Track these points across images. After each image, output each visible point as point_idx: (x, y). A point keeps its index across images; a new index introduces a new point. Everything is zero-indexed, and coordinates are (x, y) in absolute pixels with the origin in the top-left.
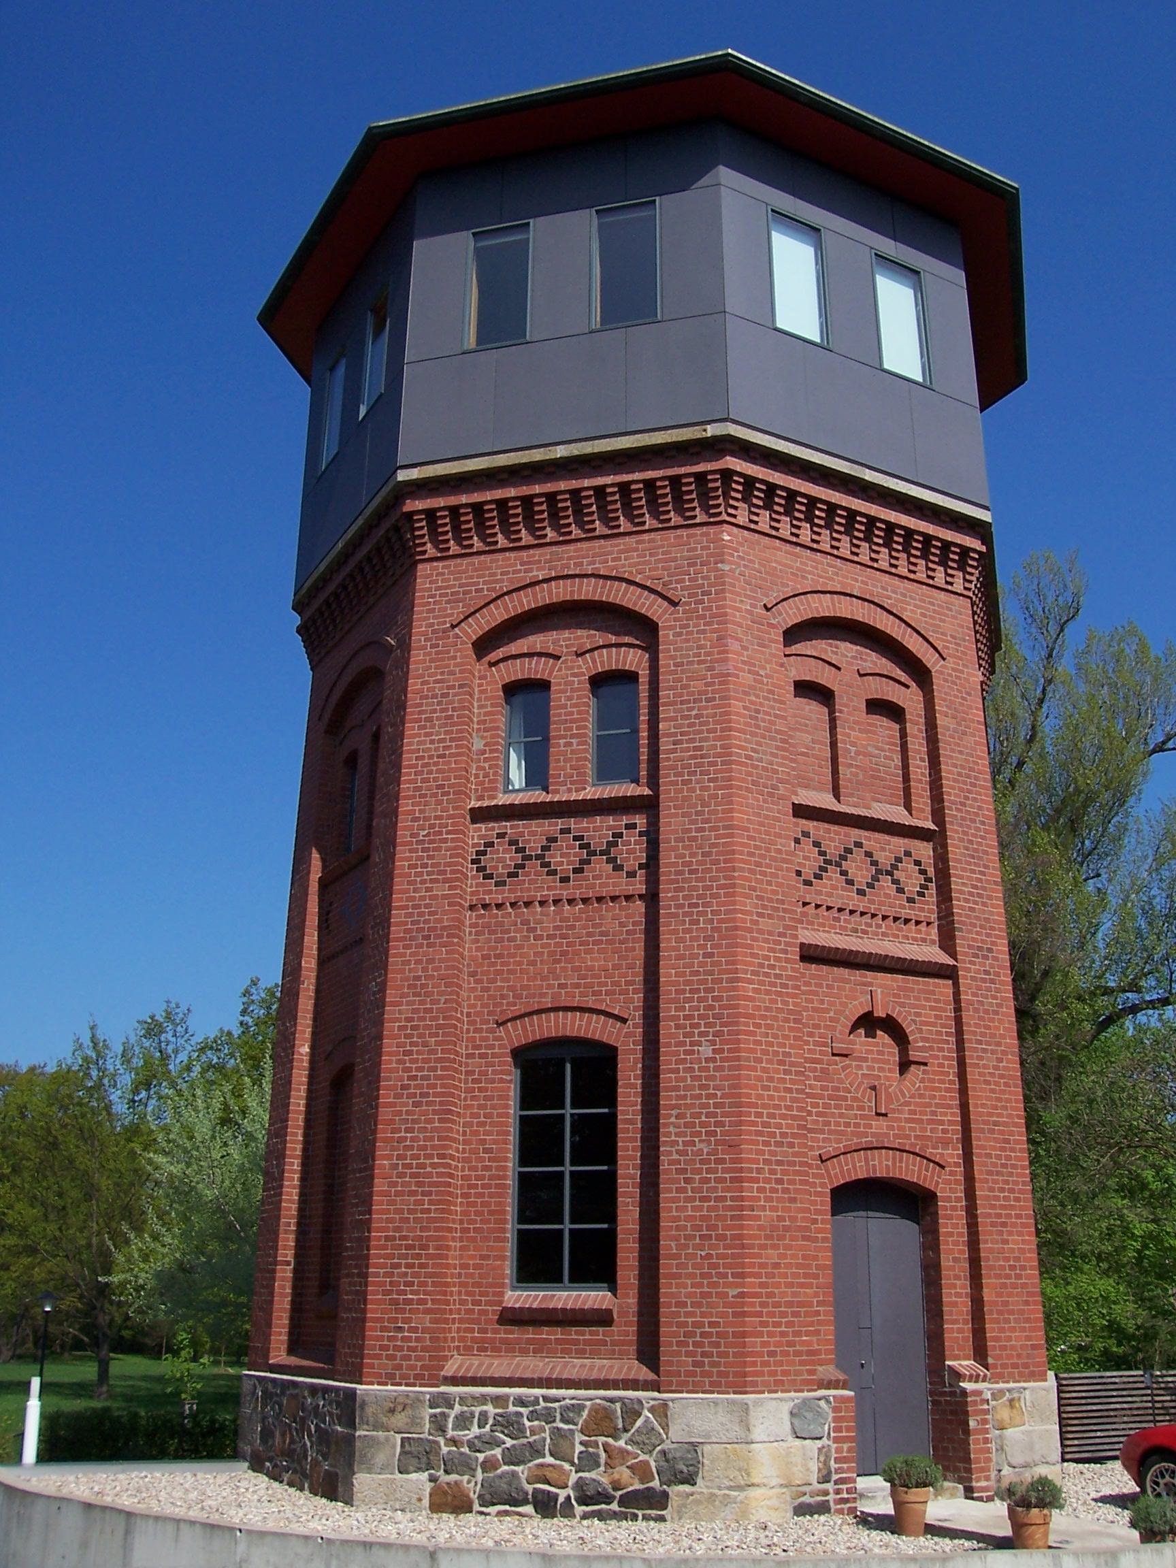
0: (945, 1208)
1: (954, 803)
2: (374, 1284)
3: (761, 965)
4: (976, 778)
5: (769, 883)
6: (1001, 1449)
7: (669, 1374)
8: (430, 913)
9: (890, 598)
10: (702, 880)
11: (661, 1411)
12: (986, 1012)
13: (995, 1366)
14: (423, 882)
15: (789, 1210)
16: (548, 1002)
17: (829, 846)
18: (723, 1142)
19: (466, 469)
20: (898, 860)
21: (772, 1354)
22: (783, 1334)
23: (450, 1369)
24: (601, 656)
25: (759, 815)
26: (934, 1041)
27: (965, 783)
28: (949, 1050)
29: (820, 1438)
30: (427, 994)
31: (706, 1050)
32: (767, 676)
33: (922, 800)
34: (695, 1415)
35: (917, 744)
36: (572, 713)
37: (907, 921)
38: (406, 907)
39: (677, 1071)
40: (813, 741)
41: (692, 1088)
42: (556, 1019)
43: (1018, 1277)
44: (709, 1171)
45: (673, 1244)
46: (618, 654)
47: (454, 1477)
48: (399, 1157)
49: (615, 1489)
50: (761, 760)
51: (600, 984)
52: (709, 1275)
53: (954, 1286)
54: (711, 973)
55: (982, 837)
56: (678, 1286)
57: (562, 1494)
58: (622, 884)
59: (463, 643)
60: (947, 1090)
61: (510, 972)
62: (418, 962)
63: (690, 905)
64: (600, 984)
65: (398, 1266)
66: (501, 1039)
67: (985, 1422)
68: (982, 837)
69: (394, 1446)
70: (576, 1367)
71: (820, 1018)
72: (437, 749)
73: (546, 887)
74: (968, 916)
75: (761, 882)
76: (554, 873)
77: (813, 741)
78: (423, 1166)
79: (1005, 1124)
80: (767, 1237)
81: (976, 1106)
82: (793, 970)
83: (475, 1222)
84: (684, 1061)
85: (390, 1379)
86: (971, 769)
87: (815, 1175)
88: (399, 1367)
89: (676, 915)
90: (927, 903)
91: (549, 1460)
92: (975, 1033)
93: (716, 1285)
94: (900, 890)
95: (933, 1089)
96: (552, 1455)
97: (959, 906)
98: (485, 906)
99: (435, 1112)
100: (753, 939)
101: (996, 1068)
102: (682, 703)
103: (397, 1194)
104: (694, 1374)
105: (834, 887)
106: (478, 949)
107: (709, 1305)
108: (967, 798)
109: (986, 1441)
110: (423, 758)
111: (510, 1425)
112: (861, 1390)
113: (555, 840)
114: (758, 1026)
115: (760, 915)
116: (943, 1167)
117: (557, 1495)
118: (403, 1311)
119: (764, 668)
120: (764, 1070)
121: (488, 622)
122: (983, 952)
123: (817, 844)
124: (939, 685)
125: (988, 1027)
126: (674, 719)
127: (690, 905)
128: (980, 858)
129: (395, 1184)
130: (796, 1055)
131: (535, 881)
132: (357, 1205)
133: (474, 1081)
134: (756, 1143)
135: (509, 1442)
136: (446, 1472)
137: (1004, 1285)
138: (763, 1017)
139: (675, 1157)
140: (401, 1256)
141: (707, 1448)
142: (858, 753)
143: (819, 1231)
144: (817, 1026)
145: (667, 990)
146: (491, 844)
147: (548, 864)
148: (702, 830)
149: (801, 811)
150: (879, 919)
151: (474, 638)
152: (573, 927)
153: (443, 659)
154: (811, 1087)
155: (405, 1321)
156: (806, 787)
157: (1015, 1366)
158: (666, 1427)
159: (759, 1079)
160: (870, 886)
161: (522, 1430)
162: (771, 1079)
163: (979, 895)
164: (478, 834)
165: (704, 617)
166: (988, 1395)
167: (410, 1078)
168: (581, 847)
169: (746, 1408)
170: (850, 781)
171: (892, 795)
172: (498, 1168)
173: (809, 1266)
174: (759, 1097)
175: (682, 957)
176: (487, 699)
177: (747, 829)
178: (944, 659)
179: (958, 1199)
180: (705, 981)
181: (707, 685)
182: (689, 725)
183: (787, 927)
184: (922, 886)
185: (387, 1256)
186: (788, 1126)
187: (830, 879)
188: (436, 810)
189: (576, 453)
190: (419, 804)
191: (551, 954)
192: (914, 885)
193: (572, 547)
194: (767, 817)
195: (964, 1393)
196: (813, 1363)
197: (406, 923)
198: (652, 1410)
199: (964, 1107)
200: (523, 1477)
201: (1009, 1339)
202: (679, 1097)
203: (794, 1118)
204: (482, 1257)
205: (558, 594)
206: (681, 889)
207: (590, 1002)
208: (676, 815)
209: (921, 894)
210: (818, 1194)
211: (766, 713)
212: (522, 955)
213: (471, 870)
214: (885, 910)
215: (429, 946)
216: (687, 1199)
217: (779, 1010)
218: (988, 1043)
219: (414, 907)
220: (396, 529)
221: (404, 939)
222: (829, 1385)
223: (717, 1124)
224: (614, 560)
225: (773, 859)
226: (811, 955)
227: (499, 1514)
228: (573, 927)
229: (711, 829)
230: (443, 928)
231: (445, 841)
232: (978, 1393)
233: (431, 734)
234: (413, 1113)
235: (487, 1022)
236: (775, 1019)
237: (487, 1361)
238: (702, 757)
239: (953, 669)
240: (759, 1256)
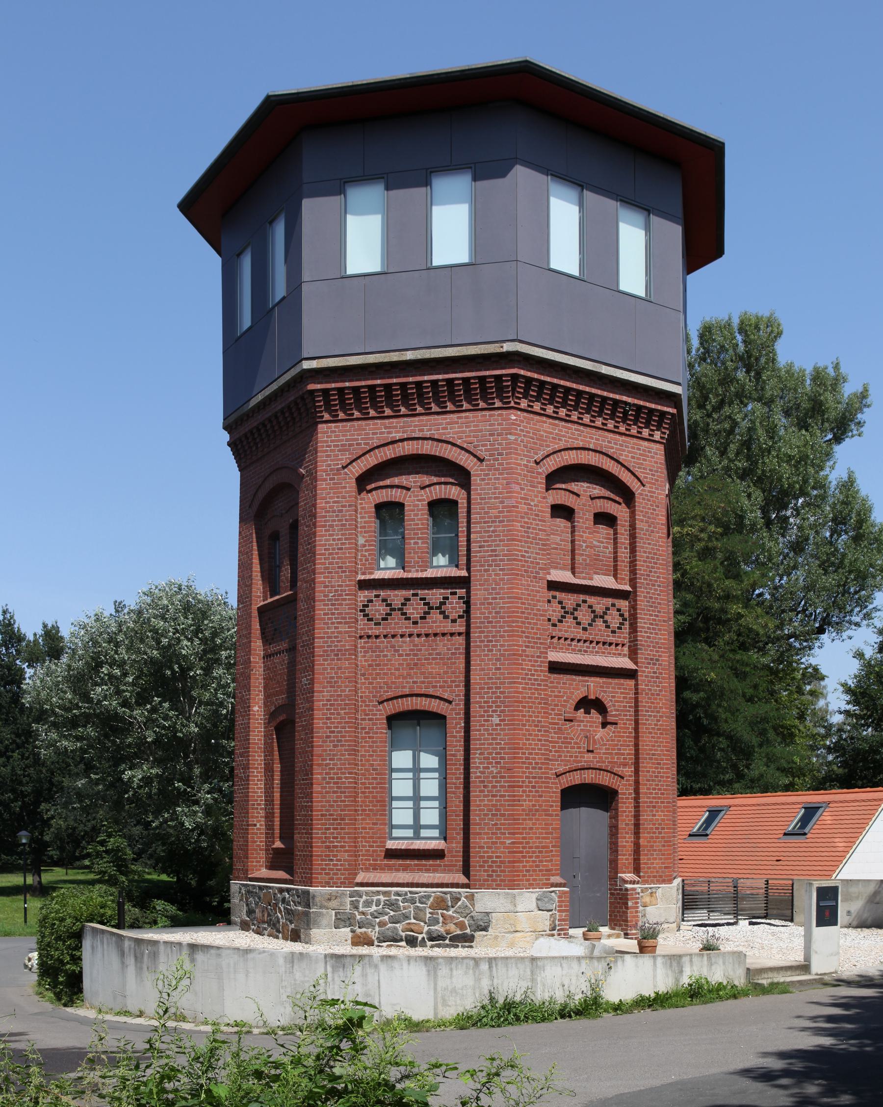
0: (622, 798)
1: (643, 575)
2: (316, 838)
3: (527, 674)
4: (658, 559)
5: (533, 628)
6: (644, 916)
7: (475, 880)
8: (338, 641)
9: (612, 448)
10: (495, 627)
11: (471, 898)
12: (653, 694)
13: (644, 877)
14: (333, 623)
15: (537, 801)
16: (407, 691)
17: (567, 604)
18: (504, 768)
19: (348, 364)
20: (608, 609)
21: (528, 871)
22: (533, 862)
23: (359, 878)
24: (435, 489)
25: (527, 590)
26: (622, 711)
27: (650, 562)
28: (630, 716)
29: (551, 910)
30: (339, 687)
31: (496, 720)
32: (535, 505)
33: (625, 573)
34: (488, 900)
35: (624, 539)
36: (418, 524)
37: (610, 644)
38: (323, 638)
39: (480, 730)
40: (561, 540)
41: (487, 739)
42: (412, 701)
43: (660, 833)
44: (496, 782)
45: (477, 818)
46: (446, 489)
47: (364, 930)
48: (327, 774)
49: (447, 934)
50: (530, 557)
51: (436, 682)
52: (496, 834)
53: (625, 838)
54: (499, 678)
55: (658, 595)
56: (480, 838)
57: (420, 937)
58: (449, 627)
59: (350, 478)
60: (627, 737)
61: (385, 674)
62: (332, 669)
63: (488, 641)
64: (436, 682)
65: (329, 829)
66: (380, 710)
67: (637, 903)
68: (658, 595)
69: (331, 916)
70: (425, 877)
71: (559, 701)
72: (337, 544)
73: (404, 627)
74: (646, 641)
75: (527, 628)
76: (409, 619)
77: (561, 540)
78: (340, 778)
79: (659, 755)
80: (527, 815)
81: (643, 745)
82: (544, 676)
83: (369, 806)
84: (484, 725)
85: (327, 884)
86: (655, 554)
87: (552, 783)
88: (332, 878)
89: (479, 647)
90: (623, 633)
91: (413, 921)
92: (645, 706)
93: (500, 838)
94: (608, 627)
95: (620, 736)
96: (414, 918)
97: (642, 636)
98: (369, 637)
99: (346, 750)
100: (523, 660)
101: (656, 725)
102: (485, 522)
103: (327, 792)
104: (488, 880)
105: (569, 627)
106: (365, 661)
107: (496, 848)
108: (651, 572)
109: (637, 912)
110: (328, 549)
111: (392, 905)
112: (573, 888)
113: (409, 600)
114: (524, 707)
115: (527, 647)
116: (622, 778)
117: (417, 938)
118: (333, 851)
119: (533, 500)
120: (527, 730)
121: (365, 465)
122: (654, 661)
123: (560, 603)
124: (639, 502)
125: (653, 703)
126: (480, 532)
127: (488, 641)
128: (656, 607)
129: (325, 788)
130: (545, 722)
131: (398, 623)
132: (303, 798)
133: (366, 733)
134: (522, 768)
135: (392, 913)
136: (359, 927)
137: (652, 837)
138: (527, 702)
139: (479, 774)
140: (330, 824)
141: (493, 914)
142: (587, 547)
143: (553, 811)
144: (557, 705)
145: (475, 688)
146: (371, 601)
147: (405, 614)
148: (495, 598)
149: (553, 586)
150: (594, 644)
151: (357, 475)
152: (421, 650)
153: (338, 488)
154: (552, 737)
155: (334, 856)
156: (556, 568)
157: (655, 877)
158: (473, 905)
159: (524, 735)
160: (590, 625)
161: (399, 907)
162: (530, 735)
163: (654, 629)
164: (364, 596)
165: (498, 469)
166: (639, 890)
167: (331, 732)
168: (424, 604)
169: (514, 897)
170: (581, 564)
171: (606, 570)
172: (381, 779)
173: (548, 829)
174: (524, 744)
175: (483, 670)
176: (365, 513)
177: (521, 598)
178: (644, 486)
179: (630, 794)
180: (496, 683)
181: (499, 512)
182: (489, 537)
183: (541, 653)
184: (620, 624)
185: (322, 824)
186: (539, 759)
187: (567, 622)
188: (338, 581)
189: (419, 357)
190: (328, 577)
191: (408, 665)
192: (616, 623)
193: (417, 419)
194: (532, 591)
195: (627, 890)
196: (549, 875)
197: (324, 647)
198: (466, 897)
199: (636, 745)
200: (400, 929)
201: (653, 863)
202: (481, 744)
203: (542, 754)
204: (373, 824)
205: (408, 449)
206: (483, 632)
207: (431, 691)
208: (480, 590)
209: (619, 628)
210: (553, 792)
211: (534, 529)
212: (391, 665)
213: (360, 616)
214: (598, 638)
215: (338, 659)
216: (485, 796)
217: (536, 698)
218: (652, 712)
219: (328, 637)
220: (302, 398)
221: (323, 656)
222: (557, 885)
223: (502, 758)
224: (443, 429)
225: (535, 615)
226: (556, 668)
227: (388, 946)
228: (421, 650)
229: (501, 598)
230: (346, 650)
231: (345, 600)
232: (634, 889)
233: (333, 535)
234: (333, 751)
235: (372, 701)
236: (534, 703)
237: (378, 875)
238: (496, 556)
239: (649, 492)
240: (522, 824)
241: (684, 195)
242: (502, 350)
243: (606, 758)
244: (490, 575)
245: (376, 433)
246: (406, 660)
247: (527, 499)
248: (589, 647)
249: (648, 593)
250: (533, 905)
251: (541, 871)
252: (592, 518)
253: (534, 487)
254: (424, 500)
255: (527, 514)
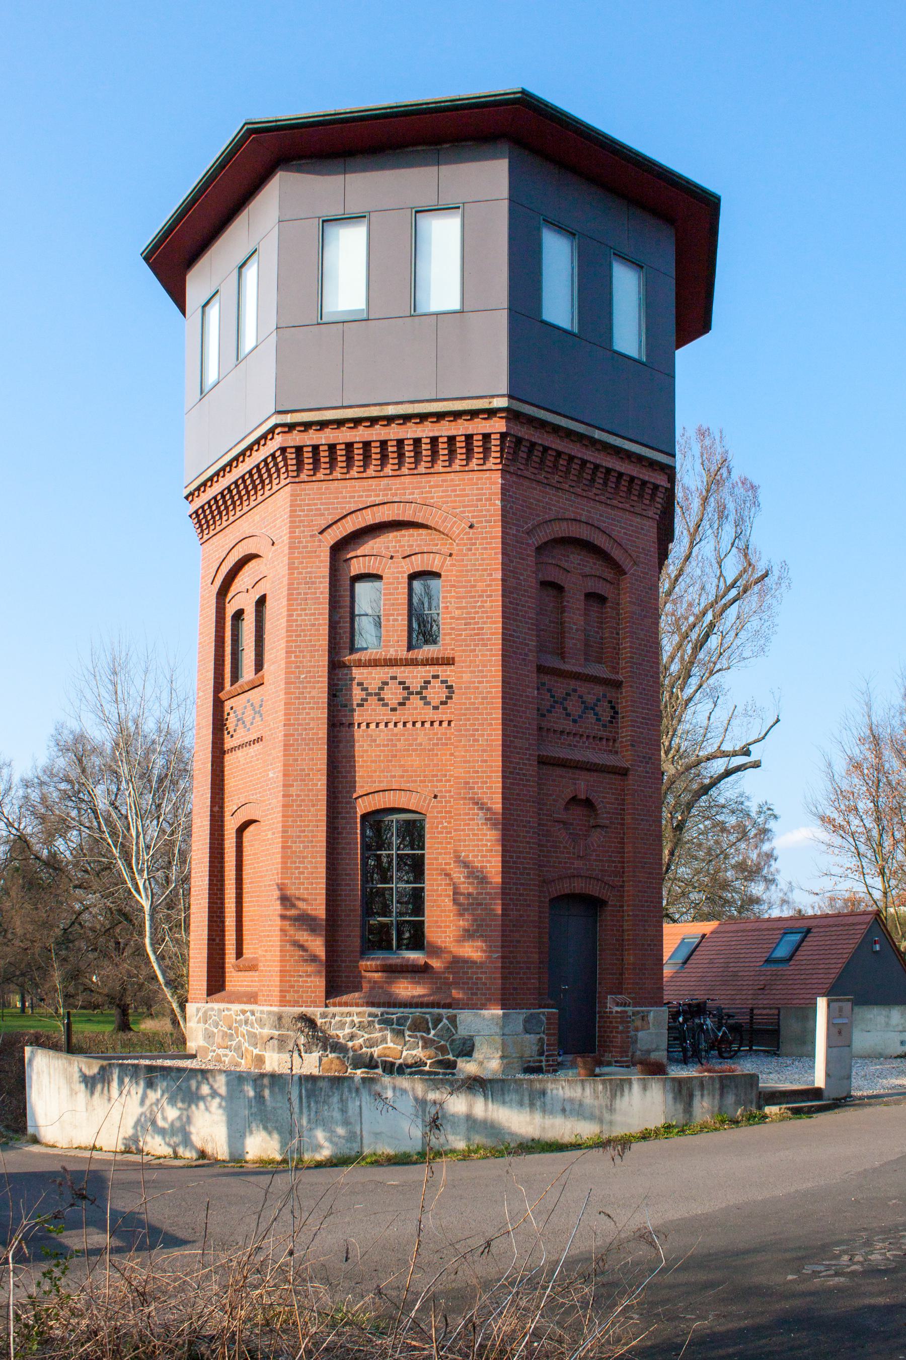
37: (601, 739)
55: (651, 686)
67: (628, 1027)
76: (386, 705)
94: (598, 720)
135: (366, 1036)
147: (383, 699)
194: (521, 675)
198: (448, 1018)
206: (469, 720)
217: (525, 795)
241: (678, 263)
242: (491, 406)
243: (597, 866)
244: (477, 656)
245: (354, 497)
246: (383, 751)
247: (517, 573)
248: (578, 742)
249: (641, 684)
250: (521, 1028)
251: (528, 989)
252: (583, 598)
253: (523, 559)
254: (404, 572)
255: (516, 588)
